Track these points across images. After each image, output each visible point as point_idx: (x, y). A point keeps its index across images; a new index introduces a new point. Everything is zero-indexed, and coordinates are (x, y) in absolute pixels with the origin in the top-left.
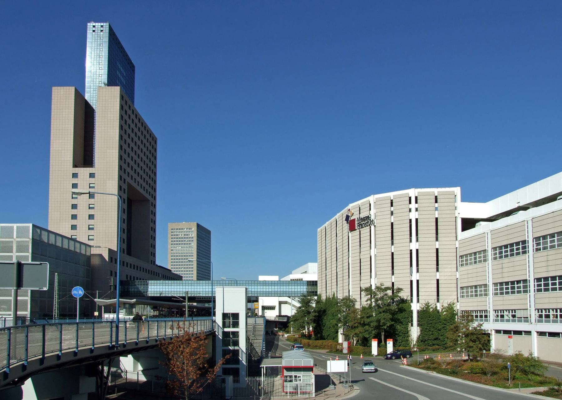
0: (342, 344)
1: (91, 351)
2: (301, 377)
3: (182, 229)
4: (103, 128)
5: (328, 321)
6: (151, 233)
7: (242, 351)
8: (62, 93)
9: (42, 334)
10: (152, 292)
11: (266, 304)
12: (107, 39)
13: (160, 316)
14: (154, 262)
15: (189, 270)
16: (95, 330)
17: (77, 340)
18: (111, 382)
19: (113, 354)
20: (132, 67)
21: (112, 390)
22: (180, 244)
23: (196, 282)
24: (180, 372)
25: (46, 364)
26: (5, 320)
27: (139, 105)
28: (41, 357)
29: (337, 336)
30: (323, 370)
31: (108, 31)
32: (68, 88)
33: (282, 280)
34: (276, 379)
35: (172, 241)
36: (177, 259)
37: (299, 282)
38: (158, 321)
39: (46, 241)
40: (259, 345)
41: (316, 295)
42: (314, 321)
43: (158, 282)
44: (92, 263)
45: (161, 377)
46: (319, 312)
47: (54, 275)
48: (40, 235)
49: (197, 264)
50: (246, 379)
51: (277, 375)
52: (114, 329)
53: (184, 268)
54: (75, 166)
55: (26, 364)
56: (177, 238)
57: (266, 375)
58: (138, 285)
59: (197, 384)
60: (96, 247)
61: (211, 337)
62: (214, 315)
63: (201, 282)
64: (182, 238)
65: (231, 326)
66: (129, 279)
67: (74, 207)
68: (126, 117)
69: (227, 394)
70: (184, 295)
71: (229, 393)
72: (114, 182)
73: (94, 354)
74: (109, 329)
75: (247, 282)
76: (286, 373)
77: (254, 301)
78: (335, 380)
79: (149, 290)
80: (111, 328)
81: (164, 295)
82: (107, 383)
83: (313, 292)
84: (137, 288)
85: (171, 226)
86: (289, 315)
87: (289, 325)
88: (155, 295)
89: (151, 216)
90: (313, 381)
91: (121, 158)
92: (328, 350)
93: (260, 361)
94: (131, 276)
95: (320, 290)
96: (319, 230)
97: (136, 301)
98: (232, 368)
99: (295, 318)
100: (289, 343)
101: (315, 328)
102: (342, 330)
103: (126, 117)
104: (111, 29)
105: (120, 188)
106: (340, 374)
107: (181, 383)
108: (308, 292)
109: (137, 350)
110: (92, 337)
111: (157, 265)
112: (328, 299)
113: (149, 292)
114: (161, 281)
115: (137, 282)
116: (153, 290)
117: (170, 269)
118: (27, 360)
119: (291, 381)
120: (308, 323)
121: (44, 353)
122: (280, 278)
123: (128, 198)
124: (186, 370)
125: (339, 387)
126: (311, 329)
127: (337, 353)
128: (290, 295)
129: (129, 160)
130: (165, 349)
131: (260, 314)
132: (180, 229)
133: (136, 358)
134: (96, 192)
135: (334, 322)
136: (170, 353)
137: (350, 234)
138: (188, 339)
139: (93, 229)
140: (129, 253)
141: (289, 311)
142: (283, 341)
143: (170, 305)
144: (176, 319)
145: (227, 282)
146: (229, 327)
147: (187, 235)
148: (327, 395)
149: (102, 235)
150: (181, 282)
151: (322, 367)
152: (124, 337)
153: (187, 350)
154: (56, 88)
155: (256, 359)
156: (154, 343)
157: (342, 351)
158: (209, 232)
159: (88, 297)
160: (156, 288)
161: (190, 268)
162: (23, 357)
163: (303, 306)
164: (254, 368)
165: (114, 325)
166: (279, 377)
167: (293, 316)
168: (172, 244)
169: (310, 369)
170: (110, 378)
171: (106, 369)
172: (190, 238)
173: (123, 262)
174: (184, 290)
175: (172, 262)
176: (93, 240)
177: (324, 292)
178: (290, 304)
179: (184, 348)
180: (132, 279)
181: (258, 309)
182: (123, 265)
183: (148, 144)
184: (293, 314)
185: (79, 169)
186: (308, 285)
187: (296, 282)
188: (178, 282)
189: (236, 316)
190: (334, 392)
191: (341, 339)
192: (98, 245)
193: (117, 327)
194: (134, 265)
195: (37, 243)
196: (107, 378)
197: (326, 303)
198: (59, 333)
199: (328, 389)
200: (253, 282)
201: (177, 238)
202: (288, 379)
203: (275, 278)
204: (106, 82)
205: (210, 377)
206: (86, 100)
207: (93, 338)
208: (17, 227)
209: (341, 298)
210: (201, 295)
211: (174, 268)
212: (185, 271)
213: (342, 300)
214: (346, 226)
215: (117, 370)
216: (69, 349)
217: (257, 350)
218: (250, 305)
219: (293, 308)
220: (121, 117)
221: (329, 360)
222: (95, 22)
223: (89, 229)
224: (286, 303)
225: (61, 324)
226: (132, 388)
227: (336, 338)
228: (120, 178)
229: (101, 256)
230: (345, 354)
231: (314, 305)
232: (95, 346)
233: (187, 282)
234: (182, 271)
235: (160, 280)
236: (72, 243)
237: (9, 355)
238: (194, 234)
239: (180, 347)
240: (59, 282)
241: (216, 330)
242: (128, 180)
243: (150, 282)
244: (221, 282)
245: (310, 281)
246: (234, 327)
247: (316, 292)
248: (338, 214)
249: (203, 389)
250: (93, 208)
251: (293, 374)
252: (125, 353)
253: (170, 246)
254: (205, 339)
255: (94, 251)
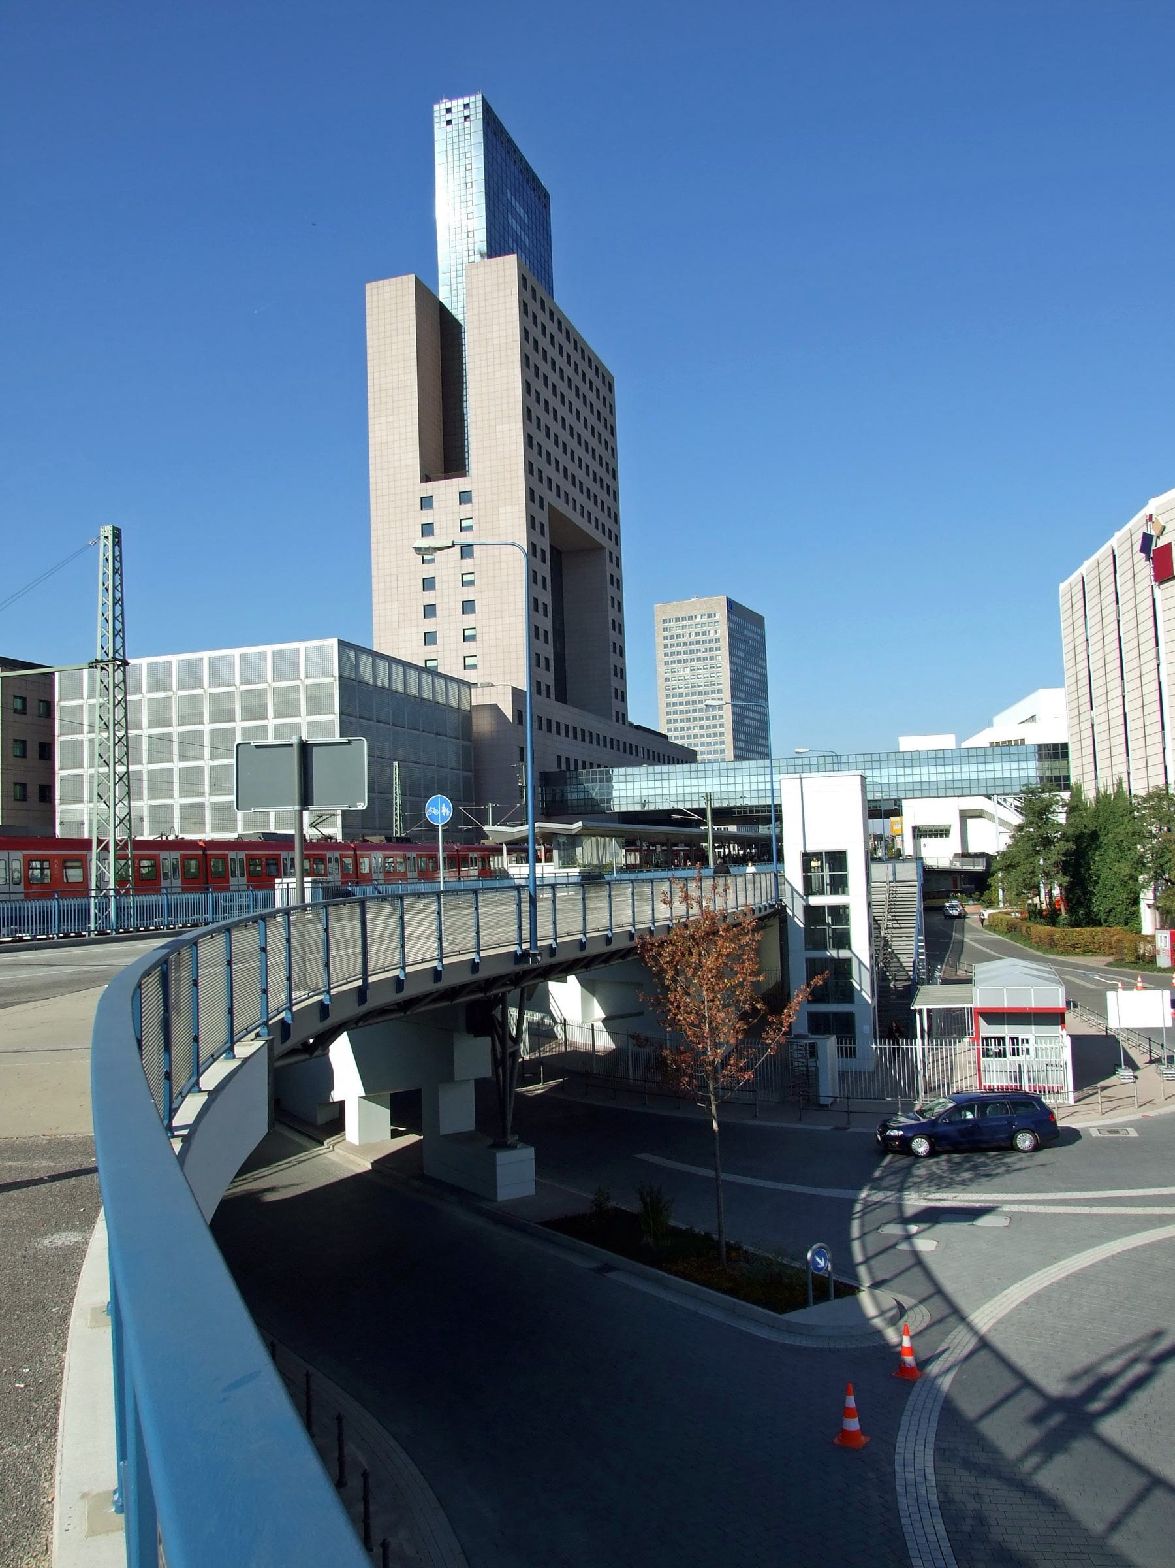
0: (1153, 937)
1: (474, 966)
2: (1032, 1041)
3: (690, 618)
4: (484, 370)
5: (1106, 868)
6: (613, 635)
7: (860, 962)
8: (387, 296)
9: (359, 922)
10: (623, 801)
11: (924, 821)
12: (479, 138)
13: (647, 863)
14: (624, 716)
15: (715, 734)
16: (480, 911)
17: (440, 939)
18: (531, 1051)
19: (526, 974)
20: (543, 197)
21: (530, 1073)
22: (686, 661)
23: (731, 766)
24: (693, 1025)
25: (373, 1002)
26: (288, 889)
27: (564, 298)
28: (360, 983)
29: (1136, 915)
30: (1095, 1019)
31: (480, 116)
32: (399, 279)
33: (964, 745)
34: (959, 1047)
35: (666, 655)
36: (681, 704)
37: (1013, 750)
38: (632, 881)
39: (370, 681)
40: (908, 947)
41: (1067, 787)
42: (1065, 868)
43: (636, 770)
44: (474, 728)
45: (647, 1040)
46: (1078, 839)
47: (391, 766)
48: (357, 666)
49: (733, 713)
50: (871, 1046)
51: (961, 1034)
52: (526, 906)
53: (701, 727)
54: (426, 478)
55: (327, 1002)
56: (678, 645)
57: (930, 1034)
58: (587, 781)
59: (740, 1058)
60: (482, 686)
61: (776, 922)
62: (780, 858)
63: (745, 763)
64: (691, 643)
65: (827, 889)
66: (564, 767)
67: (428, 584)
68: (536, 332)
69: (822, 1092)
70: (703, 805)
71: (828, 1087)
72: (516, 508)
73: (483, 974)
74: (515, 907)
75: (868, 758)
76: (986, 1030)
77: (889, 814)
78: (1134, 1054)
79: (615, 794)
80: (519, 905)
81: (652, 807)
82: (515, 1054)
83: (1058, 778)
84: (586, 791)
85: (662, 611)
86: (992, 851)
87: (991, 881)
88: (631, 809)
89: (611, 590)
90: (1067, 1055)
91: (529, 441)
92: (1111, 959)
93: (909, 993)
94: (568, 759)
95: (1078, 769)
96: (1063, 586)
97: (584, 827)
98: (836, 1014)
99: (1008, 860)
100: (995, 936)
101: (1068, 890)
102: (1150, 895)
103: (536, 332)
104: (487, 109)
105: (532, 522)
106: (1150, 1035)
107: (698, 1055)
108: (1041, 778)
109: (588, 962)
110: (474, 929)
111: (631, 725)
112: (1102, 800)
113: (615, 801)
114: (644, 769)
115: (584, 774)
116: (623, 793)
117: (664, 732)
118: (328, 992)
119: (1001, 1054)
120: (1047, 875)
121: (365, 973)
122: (959, 740)
123: (551, 547)
124: (709, 1017)
125: (1148, 1073)
126: (1056, 892)
127: (1138, 964)
128: (991, 791)
129: (548, 445)
130: (655, 959)
131: (908, 850)
132: (684, 619)
133: (588, 986)
134: (477, 540)
135: (1125, 869)
136: (666, 971)
137: (1156, 590)
138: (711, 930)
139: (473, 638)
140: (562, 697)
141: (991, 837)
142: (975, 930)
143: (666, 834)
144: (678, 873)
145: (814, 761)
146: (822, 893)
147: (704, 634)
148: (1110, 1099)
149: (490, 657)
150: (693, 766)
151: (1092, 1012)
152: (551, 927)
153: (709, 963)
154: (374, 284)
155: (900, 985)
156: (625, 944)
157: (1152, 960)
158: (758, 621)
159: (470, 822)
160: (633, 788)
161: (715, 726)
162: (322, 984)
163: (1029, 824)
164: (896, 1017)
165: (525, 895)
166: (967, 1040)
167: (1003, 855)
168: (666, 663)
169: (1054, 1017)
170: (525, 1037)
171: (514, 1012)
172: (711, 641)
173: (540, 718)
174: (702, 790)
175: (668, 713)
176: (474, 667)
177: (1090, 778)
178: (991, 817)
179: (700, 955)
180: (572, 768)
181: (902, 835)
182: (540, 728)
183: (591, 397)
184: (1002, 848)
185: (435, 483)
186: (1040, 758)
187: (1005, 750)
188: (686, 767)
189: (837, 859)
190: (1131, 1089)
191: (1148, 921)
192: (487, 680)
193: (533, 901)
194: (575, 729)
195: (350, 686)
196: (517, 1040)
197: (1097, 811)
198: (397, 920)
199: (1112, 1080)
200: (884, 757)
201: (678, 645)
202: (993, 1047)
203: (947, 742)
204: (485, 249)
205: (772, 1039)
206: (441, 304)
207: (478, 933)
208: (307, 649)
209: (1143, 793)
210: (747, 802)
211: (676, 729)
212: (702, 736)
213: (1145, 800)
214: (1145, 568)
215: (543, 1019)
216: (422, 962)
217: (903, 958)
218: (877, 825)
219: (1002, 829)
220: (525, 334)
221: (1115, 989)
222: (450, 99)
223: (465, 639)
224: (979, 814)
225: (401, 897)
226: (578, 1066)
227: (1132, 919)
228: (531, 494)
229: (494, 708)
230: (1165, 970)
231: (1062, 819)
232: (483, 954)
233: (708, 766)
234: (695, 736)
235: (640, 765)
236: (427, 679)
237: (289, 979)
238: (721, 630)
239: (691, 954)
240: (403, 786)
241: (787, 901)
242: (550, 497)
243: (616, 770)
244: (799, 762)
245: (1047, 746)
246: (834, 892)
247: (1067, 778)
248: (1118, 535)
249: (755, 1074)
250: (471, 583)
251: (1007, 1031)
252: (559, 971)
253: (661, 668)
254: (753, 931)
255: (479, 698)
